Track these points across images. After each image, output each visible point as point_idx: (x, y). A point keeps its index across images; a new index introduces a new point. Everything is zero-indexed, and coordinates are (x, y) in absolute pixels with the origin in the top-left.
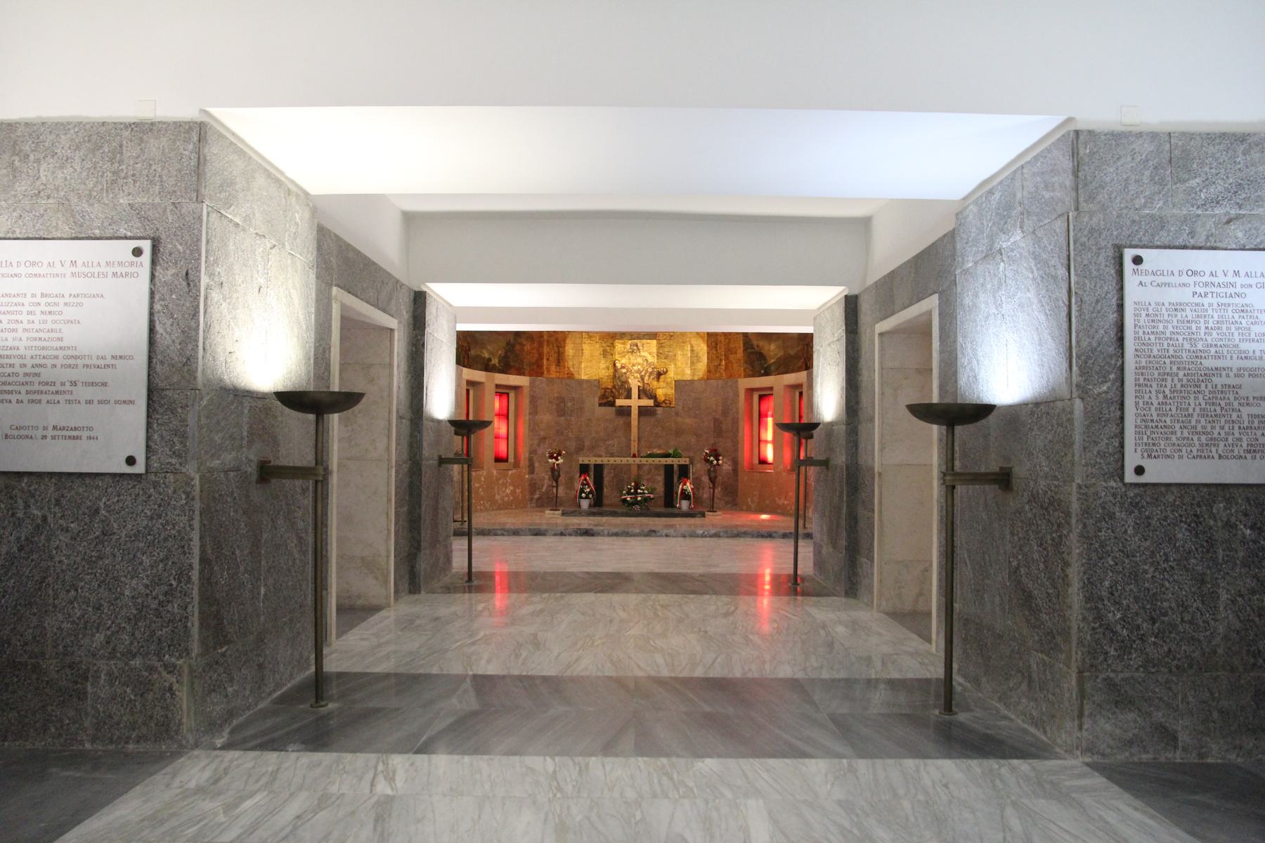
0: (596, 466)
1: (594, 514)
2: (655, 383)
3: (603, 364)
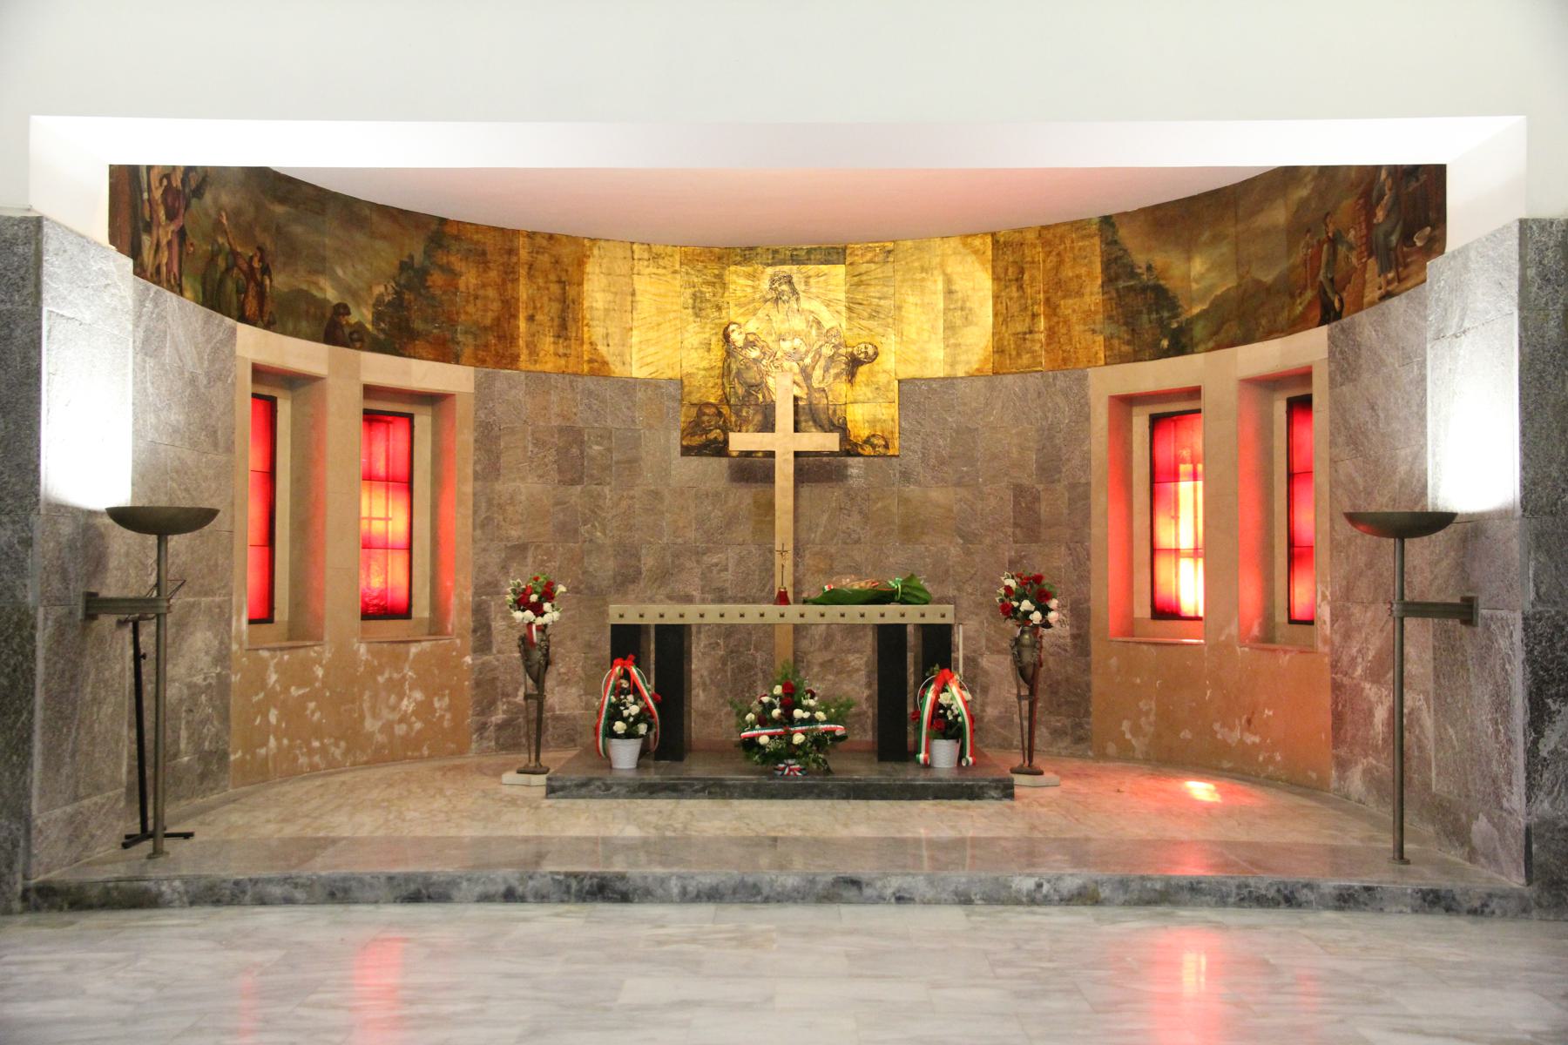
0: (662, 630)
1: (651, 790)
2: (842, 387)
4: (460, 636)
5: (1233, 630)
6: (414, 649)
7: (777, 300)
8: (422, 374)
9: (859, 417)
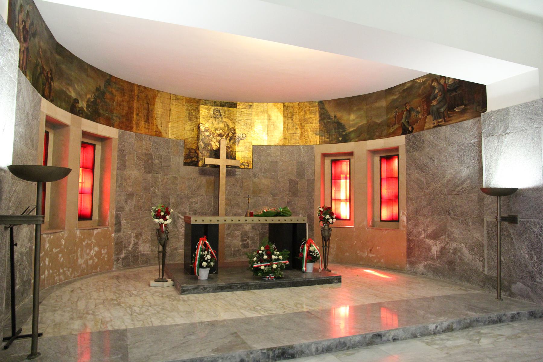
3: (188, 126)
4: (112, 227)
5: (365, 223)
6: (95, 232)
7: (215, 117)
8: (102, 130)
9: (240, 156)
